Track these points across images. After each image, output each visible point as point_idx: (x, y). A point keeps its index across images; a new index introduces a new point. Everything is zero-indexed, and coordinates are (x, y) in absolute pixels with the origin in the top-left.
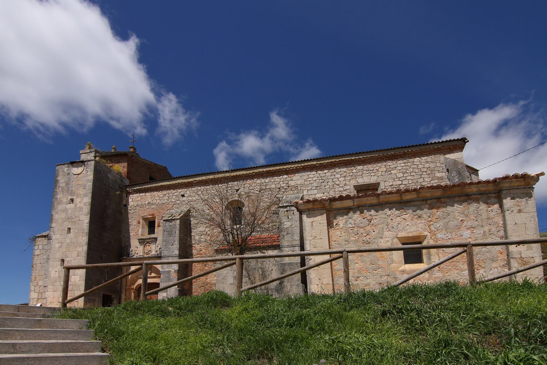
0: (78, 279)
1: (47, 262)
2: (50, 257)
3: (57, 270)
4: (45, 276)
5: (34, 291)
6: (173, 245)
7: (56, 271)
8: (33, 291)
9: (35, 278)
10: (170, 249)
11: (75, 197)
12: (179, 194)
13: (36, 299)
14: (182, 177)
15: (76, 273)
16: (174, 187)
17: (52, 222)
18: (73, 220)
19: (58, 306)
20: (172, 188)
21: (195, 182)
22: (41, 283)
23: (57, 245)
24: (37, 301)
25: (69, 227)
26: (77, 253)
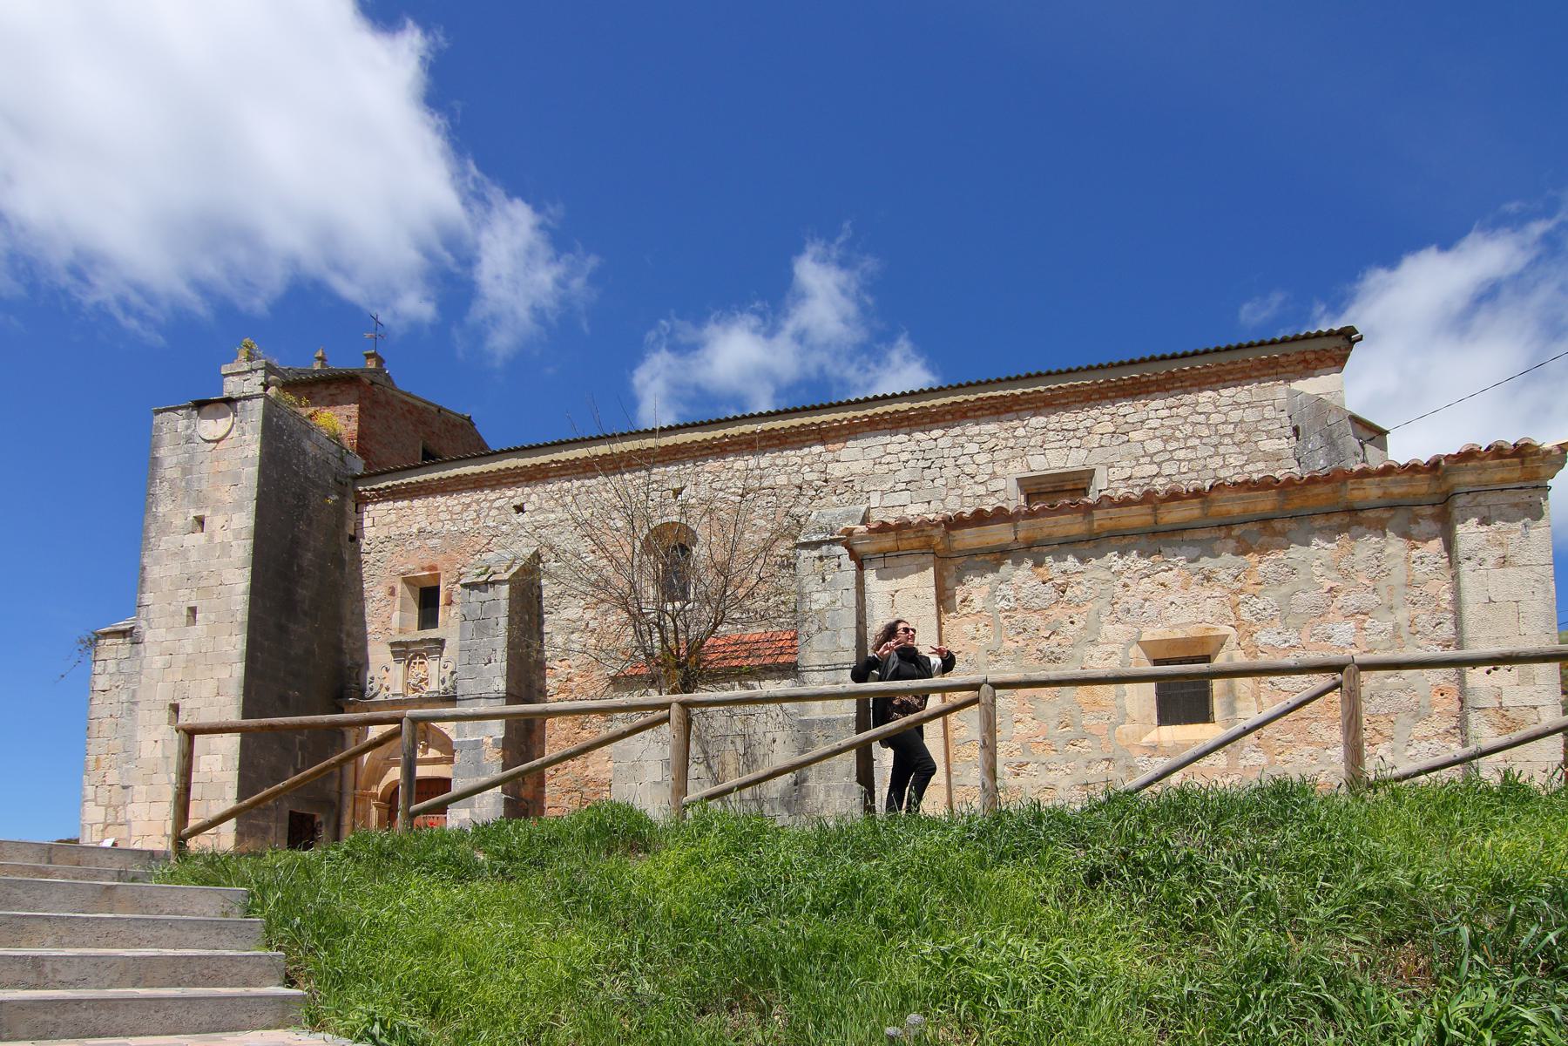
0: (218, 766)
3: (159, 738)
4: (125, 754)
5: (95, 800)
9: (97, 760)
13: (101, 827)
16: (494, 483)
23: (159, 662)
24: (102, 831)
25: (192, 604)
26: (216, 685)
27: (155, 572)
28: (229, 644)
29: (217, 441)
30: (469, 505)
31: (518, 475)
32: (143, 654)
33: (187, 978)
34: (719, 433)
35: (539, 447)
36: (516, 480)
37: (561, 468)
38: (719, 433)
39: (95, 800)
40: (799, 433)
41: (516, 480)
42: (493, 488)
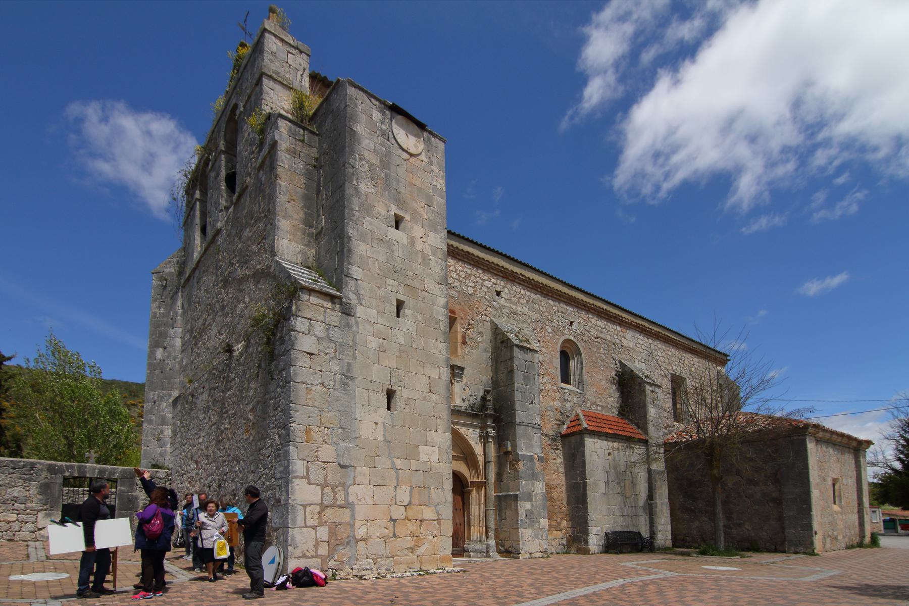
0: (435, 458)
1: (345, 386)
2: (356, 371)
3: (380, 420)
4: (341, 431)
5: (307, 477)
6: (532, 403)
7: (376, 423)
8: (302, 477)
9: (308, 431)
10: (527, 409)
11: (407, 217)
12: (492, 286)
13: (318, 508)
14: (480, 245)
15: (429, 439)
16: (486, 268)
17: (352, 261)
18: (409, 282)
19: (387, 531)
20: (482, 267)
21: (521, 277)
22: (327, 453)
23: (373, 343)
24: (319, 513)
25: (402, 298)
26: (428, 382)
27: (361, 248)
28: (436, 348)
29: (411, 155)
30: (470, 276)
31: (501, 271)
32: (355, 328)
33: (47, 455)
34: (591, 301)
35: (555, 278)
36: (499, 273)
37: (523, 280)
38: (591, 301)
39: (307, 477)
40: (615, 318)
41: (499, 273)
42: (484, 270)
